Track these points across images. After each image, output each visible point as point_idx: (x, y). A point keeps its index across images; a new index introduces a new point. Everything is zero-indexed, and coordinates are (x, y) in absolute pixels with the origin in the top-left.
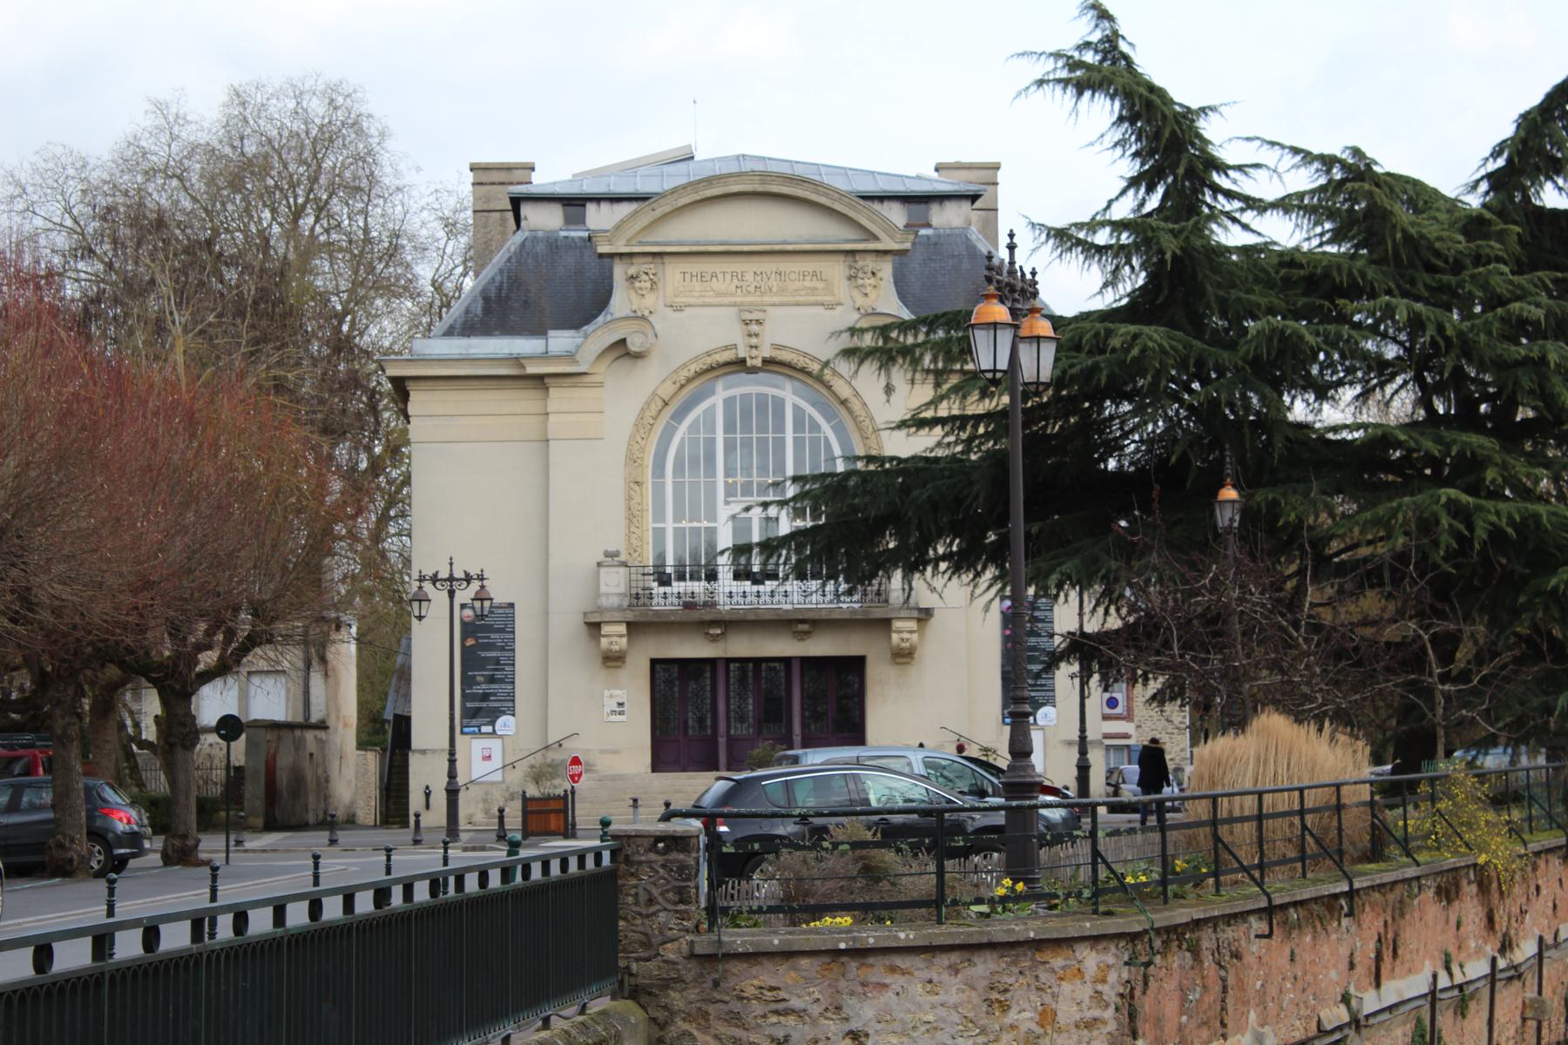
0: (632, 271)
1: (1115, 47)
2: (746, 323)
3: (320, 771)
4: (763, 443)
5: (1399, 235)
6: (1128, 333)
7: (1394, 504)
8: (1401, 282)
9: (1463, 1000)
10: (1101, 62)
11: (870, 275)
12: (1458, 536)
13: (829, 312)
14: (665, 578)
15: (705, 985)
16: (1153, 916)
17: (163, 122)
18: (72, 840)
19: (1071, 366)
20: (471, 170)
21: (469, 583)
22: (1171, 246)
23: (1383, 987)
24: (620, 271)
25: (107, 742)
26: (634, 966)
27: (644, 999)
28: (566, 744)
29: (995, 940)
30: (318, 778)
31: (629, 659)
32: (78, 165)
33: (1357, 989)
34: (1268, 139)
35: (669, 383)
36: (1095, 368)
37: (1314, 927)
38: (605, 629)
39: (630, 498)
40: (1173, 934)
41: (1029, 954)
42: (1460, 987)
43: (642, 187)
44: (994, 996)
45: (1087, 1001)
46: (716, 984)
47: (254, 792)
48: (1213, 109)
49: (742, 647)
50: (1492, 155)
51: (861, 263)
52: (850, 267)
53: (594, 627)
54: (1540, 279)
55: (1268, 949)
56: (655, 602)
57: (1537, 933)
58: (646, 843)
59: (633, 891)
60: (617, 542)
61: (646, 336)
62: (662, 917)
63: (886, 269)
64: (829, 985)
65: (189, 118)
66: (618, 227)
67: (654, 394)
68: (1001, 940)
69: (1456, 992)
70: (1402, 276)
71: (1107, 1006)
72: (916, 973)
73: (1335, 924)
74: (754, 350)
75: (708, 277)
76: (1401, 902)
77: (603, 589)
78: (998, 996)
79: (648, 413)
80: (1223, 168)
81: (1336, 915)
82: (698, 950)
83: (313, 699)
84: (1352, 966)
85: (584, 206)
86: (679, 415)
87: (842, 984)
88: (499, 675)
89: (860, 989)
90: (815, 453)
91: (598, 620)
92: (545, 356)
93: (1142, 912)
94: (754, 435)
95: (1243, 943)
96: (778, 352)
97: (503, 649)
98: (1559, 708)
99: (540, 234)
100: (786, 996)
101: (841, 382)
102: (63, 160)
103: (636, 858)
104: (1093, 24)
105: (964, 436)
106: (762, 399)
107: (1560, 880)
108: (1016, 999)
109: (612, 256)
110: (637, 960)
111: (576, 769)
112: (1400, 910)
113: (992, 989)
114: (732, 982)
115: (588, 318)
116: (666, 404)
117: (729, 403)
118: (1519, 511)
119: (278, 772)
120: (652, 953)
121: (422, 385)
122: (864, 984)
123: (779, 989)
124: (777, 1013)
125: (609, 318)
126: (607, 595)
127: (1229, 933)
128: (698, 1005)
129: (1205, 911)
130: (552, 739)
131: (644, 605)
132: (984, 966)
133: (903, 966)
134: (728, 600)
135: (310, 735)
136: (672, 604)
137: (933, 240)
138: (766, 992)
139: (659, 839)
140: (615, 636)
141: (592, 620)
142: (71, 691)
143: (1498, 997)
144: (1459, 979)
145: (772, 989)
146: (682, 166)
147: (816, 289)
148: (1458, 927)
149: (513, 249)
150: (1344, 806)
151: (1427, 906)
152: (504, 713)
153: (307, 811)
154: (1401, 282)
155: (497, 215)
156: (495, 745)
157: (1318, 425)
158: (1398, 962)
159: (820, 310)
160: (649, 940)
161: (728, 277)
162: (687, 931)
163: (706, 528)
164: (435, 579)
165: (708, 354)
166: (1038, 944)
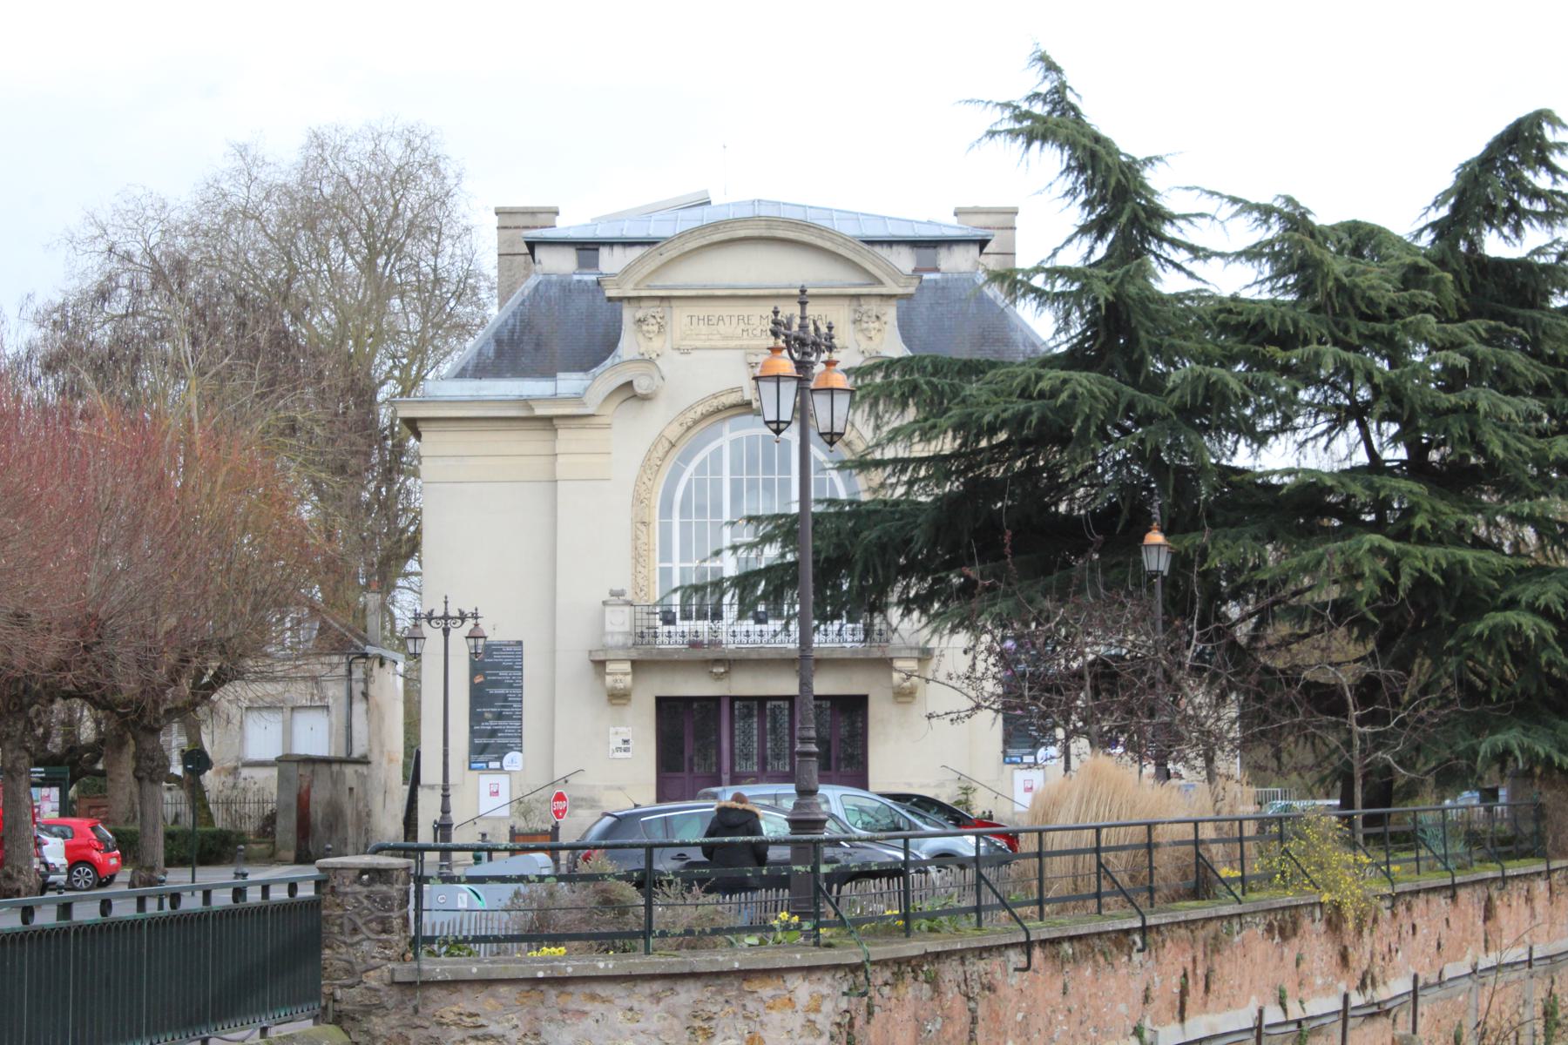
0: (640, 314)
1: (1063, 98)
3: (361, 805)
5: (1330, 284)
6: (1058, 377)
7: (1320, 550)
8: (1335, 330)
9: (1301, 1035)
10: (1050, 113)
11: (874, 318)
12: (1383, 583)
14: (670, 617)
15: (406, 1011)
16: (870, 949)
17: (242, 163)
18: (20, 872)
19: (1004, 411)
20: (497, 214)
21: (463, 622)
22: (1104, 292)
23: (1187, 1023)
24: (628, 314)
25: (121, 775)
26: (338, 994)
27: (347, 1024)
28: (572, 780)
29: (696, 970)
30: (359, 814)
31: (634, 697)
32: (157, 206)
33: (1154, 1022)
34: (1207, 189)
35: (676, 424)
36: (1028, 412)
37: (1096, 962)
38: (610, 667)
39: (637, 538)
40: (901, 967)
41: (736, 984)
42: (1299, 1022)
43: (653, 231)
44: (698, 1023)
45: (798, 1029)
46: (416, 1011)
47: (286, 828)
48: (1159, 159)
49: (745, 685)
50: (1434, 204)
51: (865, 308)
52: (855, 311)
53: (600, 664)
54: (1472, 327)
55: (1032, 982)
56: (659, 640)
57: (1412, 971)
58: (352, 875)
59: (338, 922)
60: (623, 582)
61: (652, 378)
62: (366, 946)
63: (891, 313)
64: (529, 1012)
65: (267, 160)
66: (625, 271)
67: (661, 435)
68: (703, 970)
69: (1293, 1027)
70: (1337, 324)
71: (821, 1034)
72: (617, 1001)
73: (1125, 959)
75: (714, 321)
76: (1216, 938)
77: (609, 628)
78: (701, 1024)
79: (655, 455)
80: (1170, 218)
81: (1126, 950)
82: (398, 978)
83: (355, 734)
84: (1147, 999)
85: (597, 250)
86: (686, 458)
87: (541, 1011)
88: (506, 711)
89: (559, 1016)
91: (602, 658)
92: (554, 399)
93: (859, 944)
95: (999, 976)
97: (510, 686)
98: (1481, 754)
99: (554, 278)
100: (484, 1022)
102: (143, 201)
103: (342, 889)
104: (1041, 74)
105: (905, 478)
107: (1447, 920)
108: (721, 1026)
109: (621, 299)
110: (342, 987)
111: (561, 805)
112: (1215, 946)
113: (695, 1017)
114: (432, 1008)
115: (597, 362)
116: (673, 445)
117: (735, 443)
118: (1446, 557)
119: (312, 807)
120: (356, 980)
121: (434, 425)
122: (563, 1012)
123: (477, 1015)
124: (476, 1038)
125: (617, 360)
126: (612, 634)
127: (980, 966)
128: (399, 1030)
129: (943, 944)
130: (558, 775)
131: (649, 643)
132: (687, 995)
133: (603, 995)
134: (731, 639)
135: (349, 770)
136: (833, 641)
137: (941, 284)
138: (464, 1018)
139: (363, 871)
140: (620, 676)
141: (597, 658)
142: (20, 725)
143: (1350, 1034)
144: (1295, 1012)
145: (471, 1015)
146: (697, 211)
148: (1298, 965)
149: (526, 293)
150: (1157, 845)
151: (1255, 942)
152: (511, 749)
153: (346, 845)
154: (1335, 330)
156: (502, 781)
157: (1259, 470)
158: (1211, 996)
160: (353, 967)
161: (734, 320)
162: (389, 959)
164: (430, 617)
165: (715, 396)
166: (746, 975)
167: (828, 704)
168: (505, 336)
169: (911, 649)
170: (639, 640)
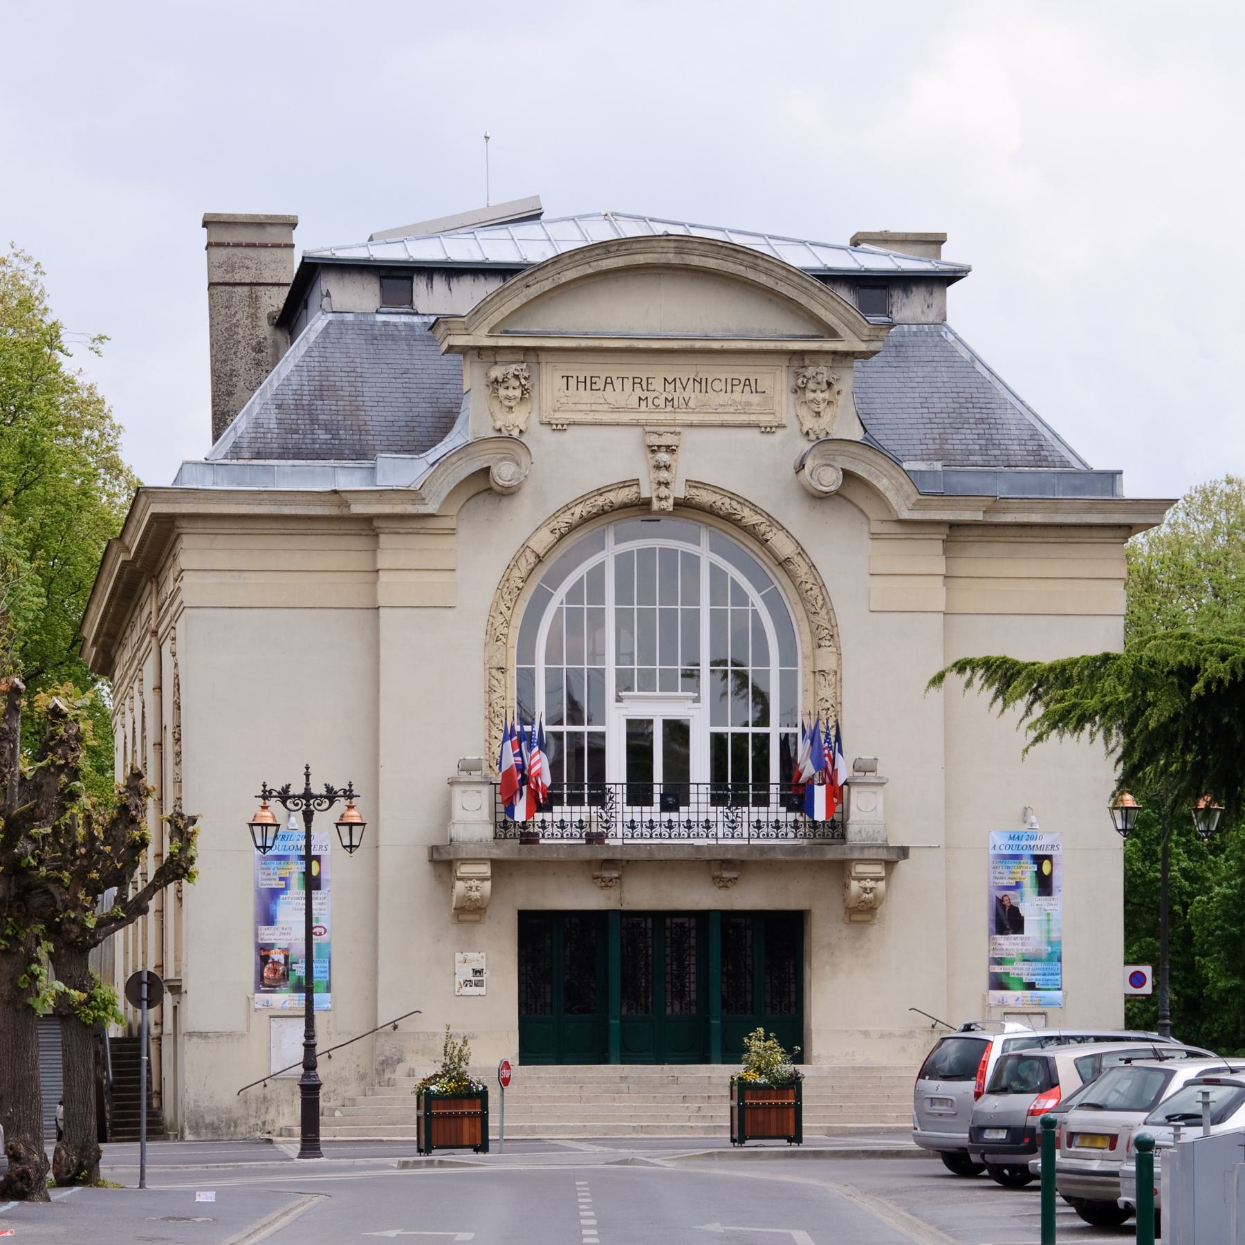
0: (497, 372)
2: (654, 449)
4: (669, 616)
11: (824, 386)
13: (766, 437)
21: (331, 803)
39: (491, 690)
51: (810, 372)
52: (797, 375)
66: (477, 311)
67: (525, 546)
74: (663, 487)
79: (516, 573)
85: (411, 279)
86: (554, 580)
90: (740, 637)
94: (586, 606)
96: (694, 492)
101: (781, 534)
106: (669, 554)
116: (540, 560)
117: (623, 562)
130: (384, 1018)
136: (571, 836)
147: (749, 404)
155: (246, 289)
159: (754, 434)
161: (628, 383)
163: (755, 735)
165: (600, 492)
167: (693, 922)
168: (289, 401)
169: (879, 847)
170: (501, 832)
